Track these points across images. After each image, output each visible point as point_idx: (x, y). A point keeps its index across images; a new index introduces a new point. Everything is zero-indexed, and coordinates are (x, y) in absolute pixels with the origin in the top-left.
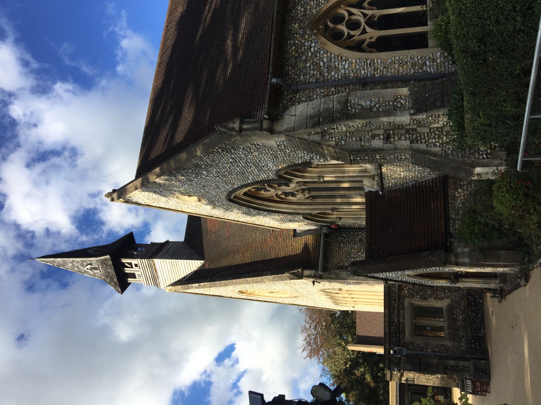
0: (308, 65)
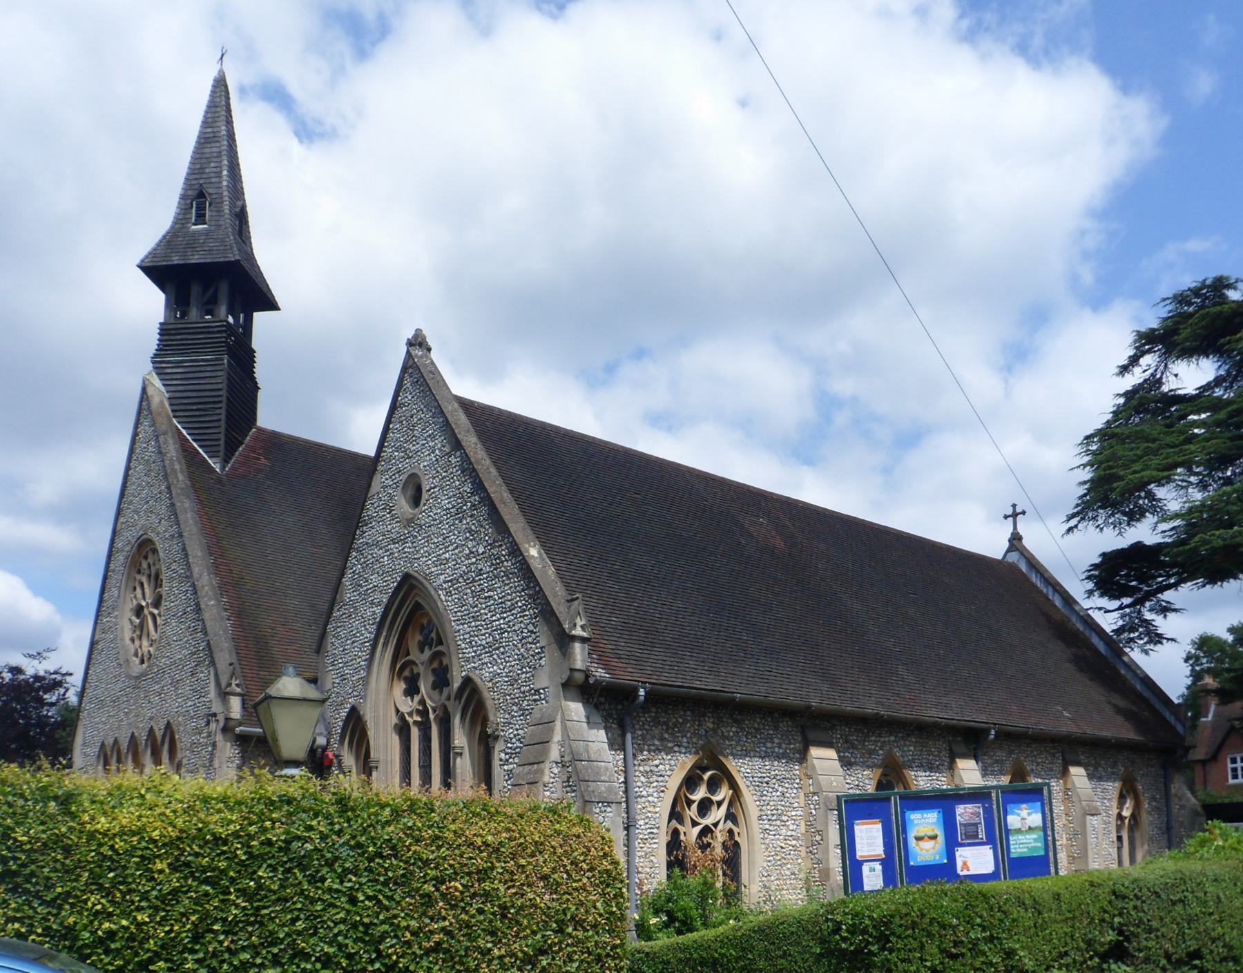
0: (657, 742)
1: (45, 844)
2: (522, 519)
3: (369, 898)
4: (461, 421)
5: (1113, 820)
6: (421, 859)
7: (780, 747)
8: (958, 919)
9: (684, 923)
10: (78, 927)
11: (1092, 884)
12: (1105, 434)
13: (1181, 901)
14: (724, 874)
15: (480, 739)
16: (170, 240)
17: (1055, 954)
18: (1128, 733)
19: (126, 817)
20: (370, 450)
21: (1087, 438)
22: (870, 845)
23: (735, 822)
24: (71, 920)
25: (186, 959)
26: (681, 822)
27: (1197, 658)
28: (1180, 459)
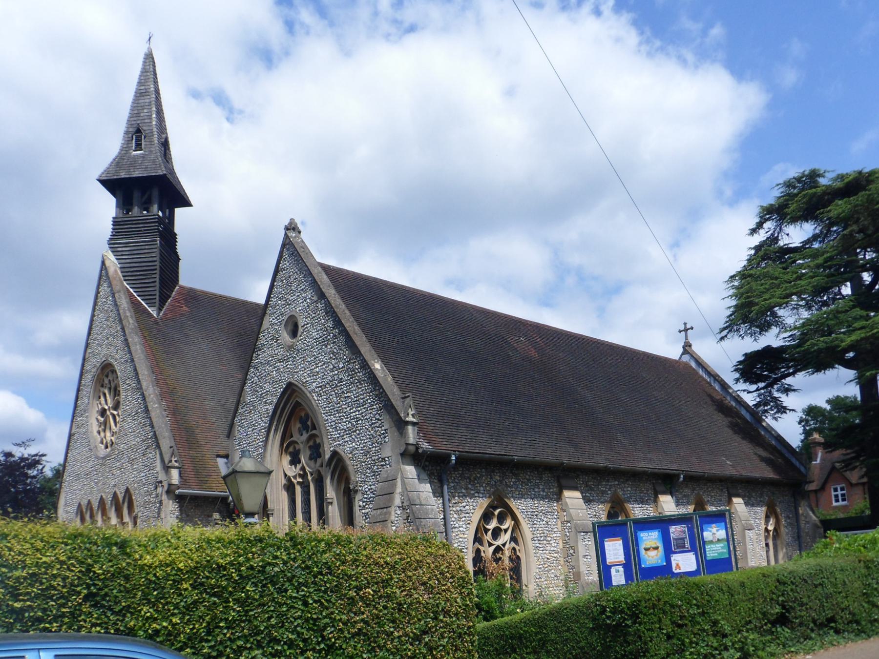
1: (113, 575)
2: (368, 344)
3: (315, 602)
4: (324, 280)
6: (346, 575)
8: (682, 601)
9: (487, 612)
10: (136, 628)
11: (764, 576)
12: (743, 275)
13: (820, 584)
14: (511, 578)
15: (344, 492)
16: (118, 162)
17: (743, 622)
18: (768, 473)
19: (162, 555)
20: (262, 301)
21: (732, 277)
24: (132, 623)
25: (203, 646)
26: (481, 544)
27: (807, 421)
28: (794, 291)
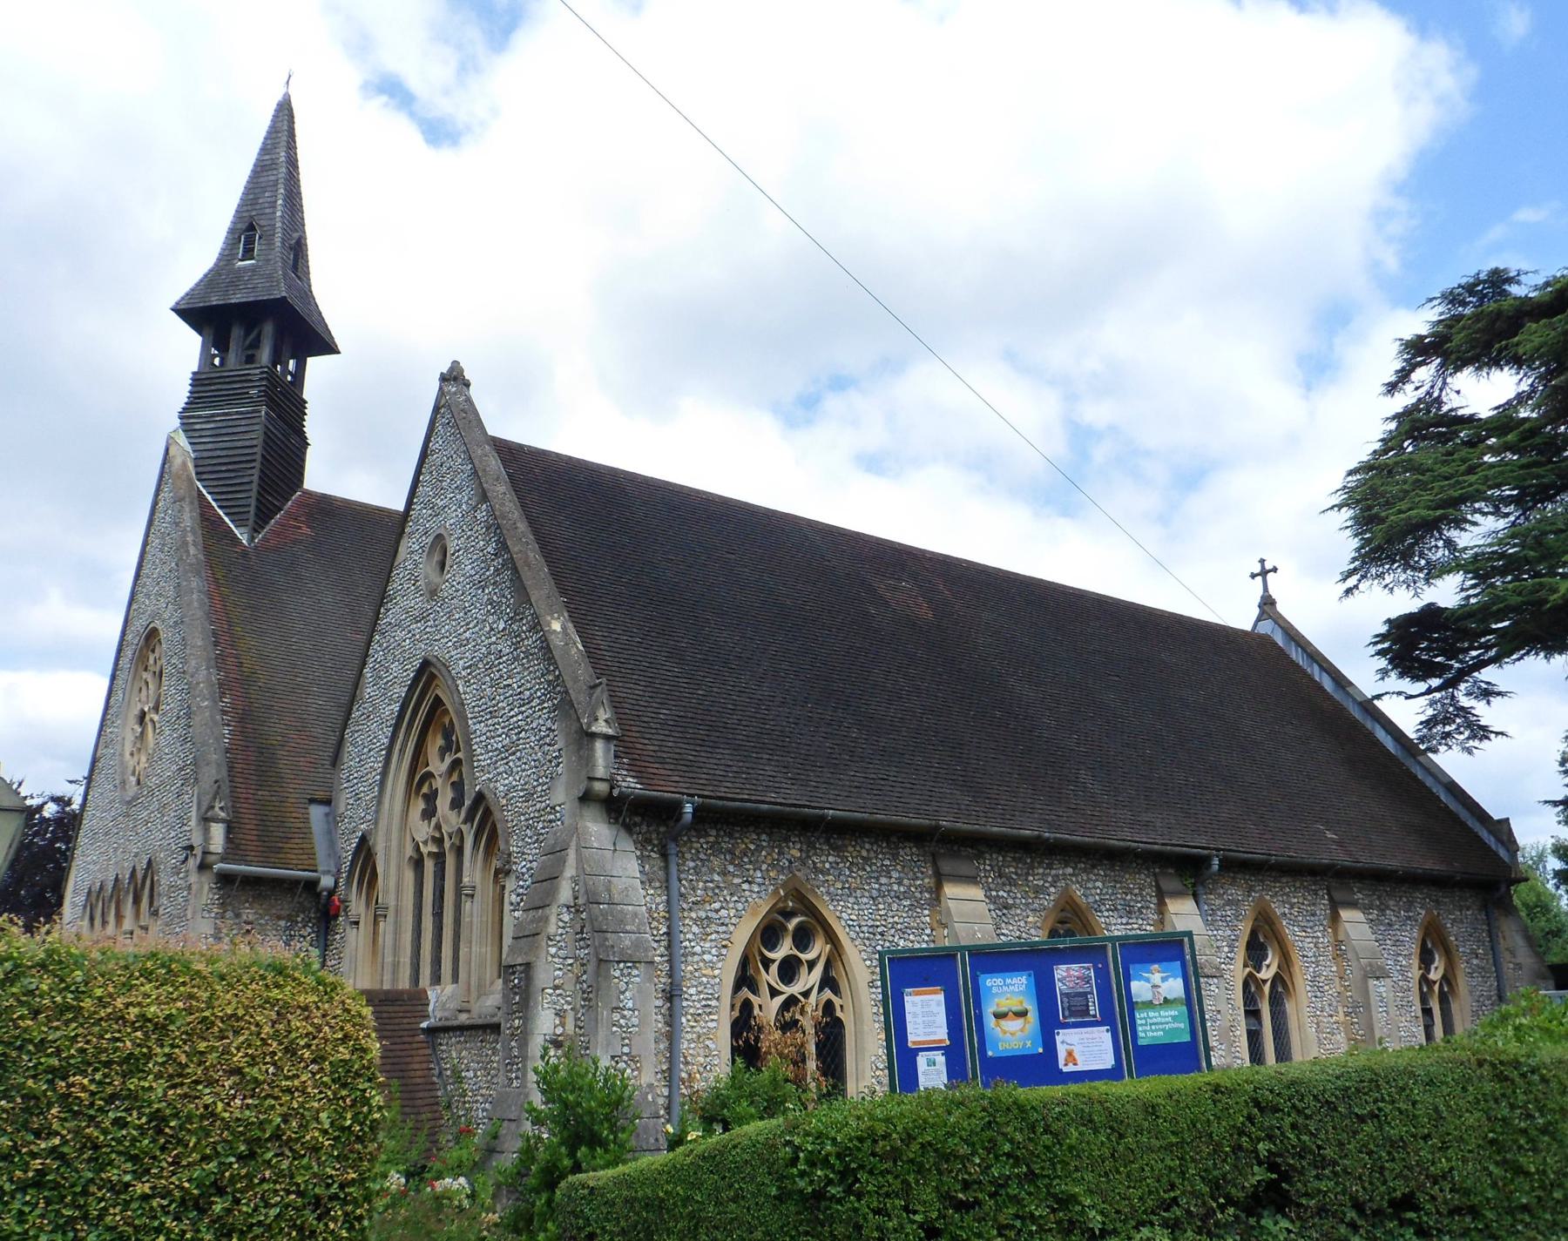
0: (716, 877)
4: (494, 464)
5: (1414, 985)
7: (900, 883)
12: (1365, 468)
13: (1373, 1116)
16: (211, 280)
20: (399, 505)
22: (928, 1025)
23: (836, 990)
26: (755, 991)
